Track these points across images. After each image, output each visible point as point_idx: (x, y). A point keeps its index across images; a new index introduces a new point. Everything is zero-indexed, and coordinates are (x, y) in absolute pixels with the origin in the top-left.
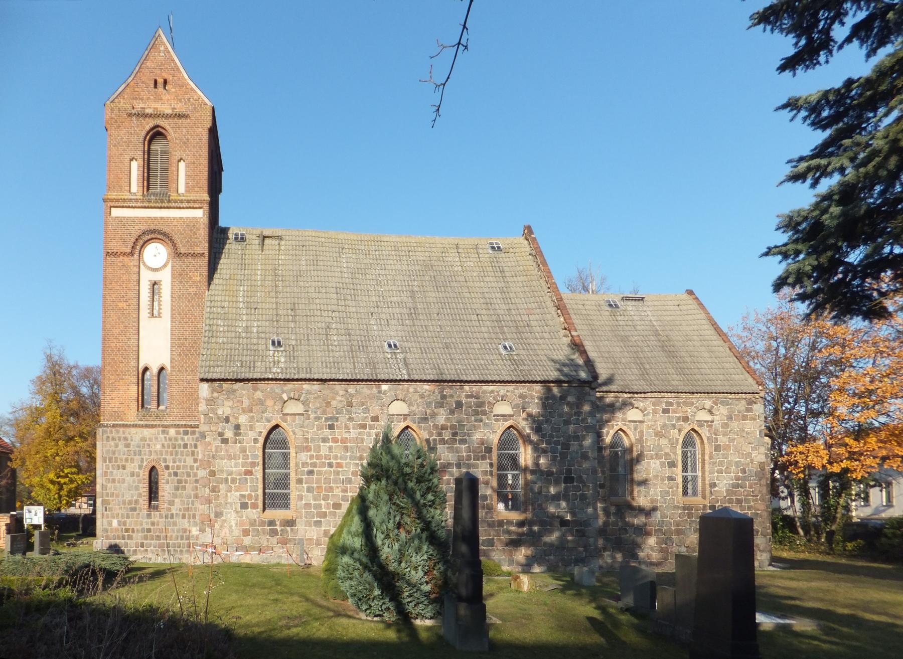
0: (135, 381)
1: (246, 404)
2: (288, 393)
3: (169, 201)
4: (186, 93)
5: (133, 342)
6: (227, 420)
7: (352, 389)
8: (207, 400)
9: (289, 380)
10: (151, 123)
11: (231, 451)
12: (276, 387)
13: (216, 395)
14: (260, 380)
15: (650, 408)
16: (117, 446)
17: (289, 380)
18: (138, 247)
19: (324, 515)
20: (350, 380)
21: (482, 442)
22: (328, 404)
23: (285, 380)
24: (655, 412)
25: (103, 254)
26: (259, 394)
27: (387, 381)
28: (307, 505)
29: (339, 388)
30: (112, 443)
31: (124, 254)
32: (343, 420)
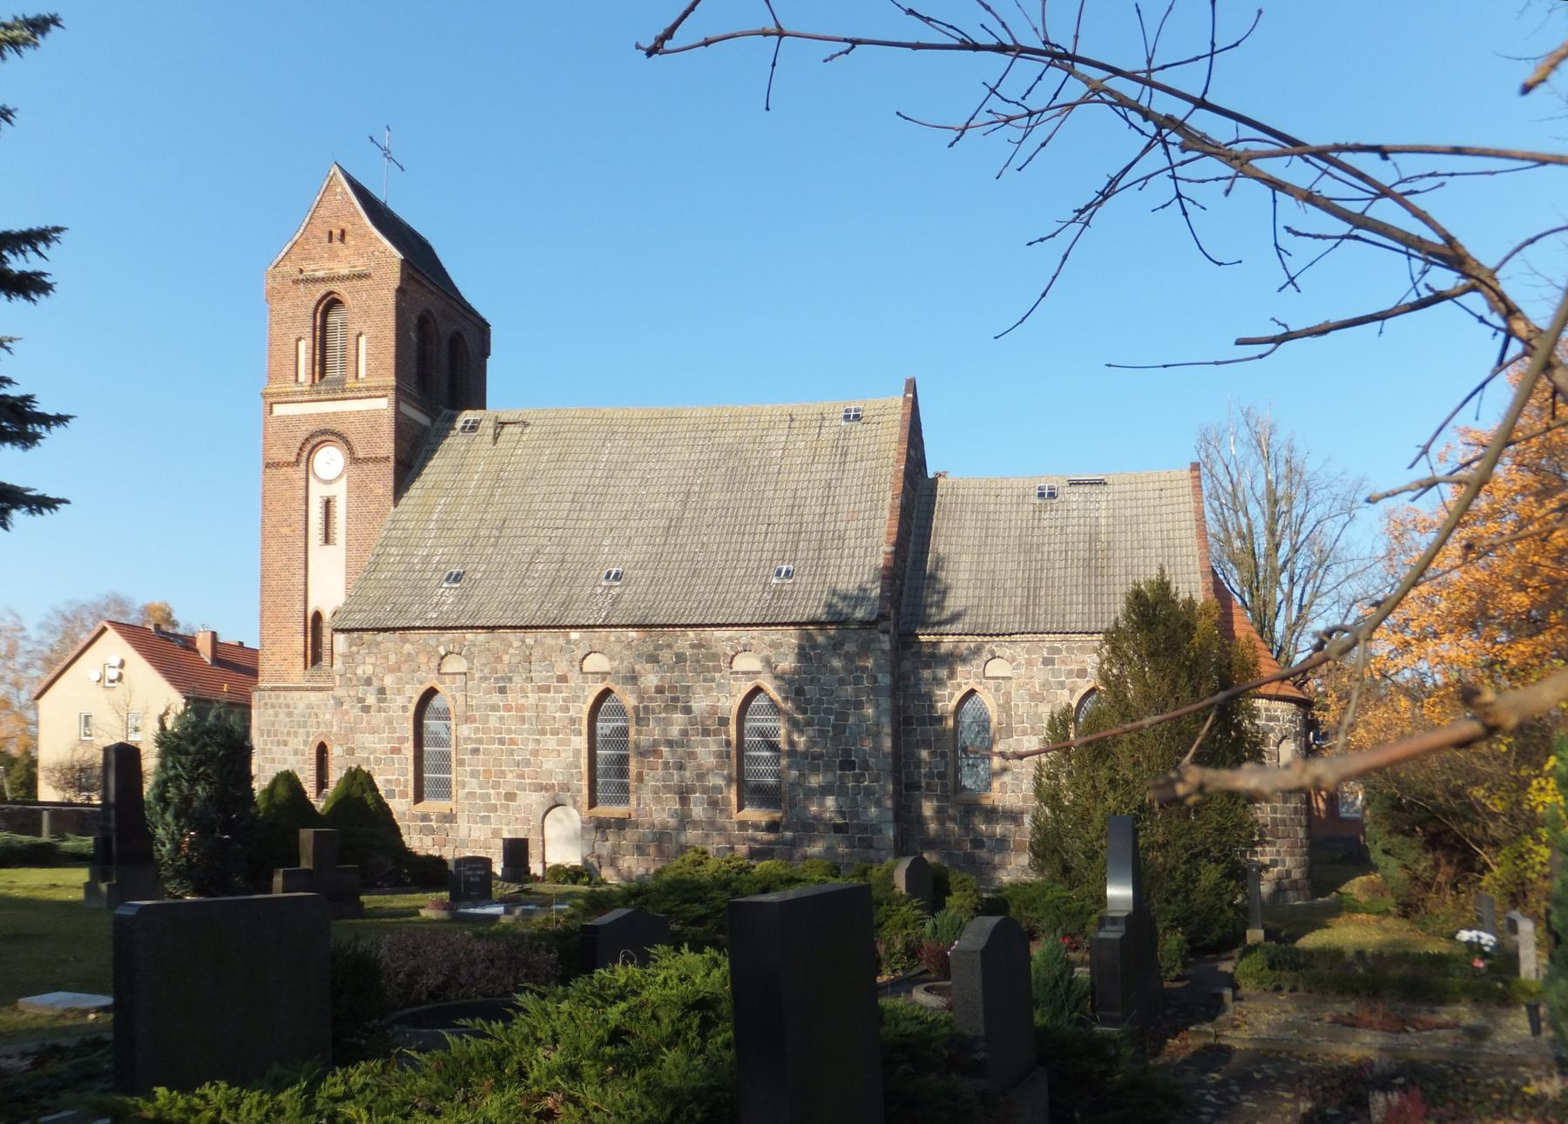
0: (301, 629)
1: (393, 659)
2: (446, 644)
3: (344, 391)
4: (370, 245)
5: (300, 579)
6: (368, 682)
7: (530, 638)
8: (343, 656)
9: (446, 628)
10: (320, 290)
11: (374, 722)
12: (430, 638)
13: (354, 649)
14: (409, 628)
15: (1022, 658)
16: (276, 715)
17: (446, 628)
18: (305, 454)
19: (494, 808)
20: (527, 627)
21: (713, 710)
22: (499, 659)
23: (440, 628)
24: (1030, 663)
25: (261, 467)
26: (408, 648)
27: (577, 627)
28: (471, 795)
29: (514, 637)
30: (271, 712)
31: (288, 464)
32: (518, 680)
